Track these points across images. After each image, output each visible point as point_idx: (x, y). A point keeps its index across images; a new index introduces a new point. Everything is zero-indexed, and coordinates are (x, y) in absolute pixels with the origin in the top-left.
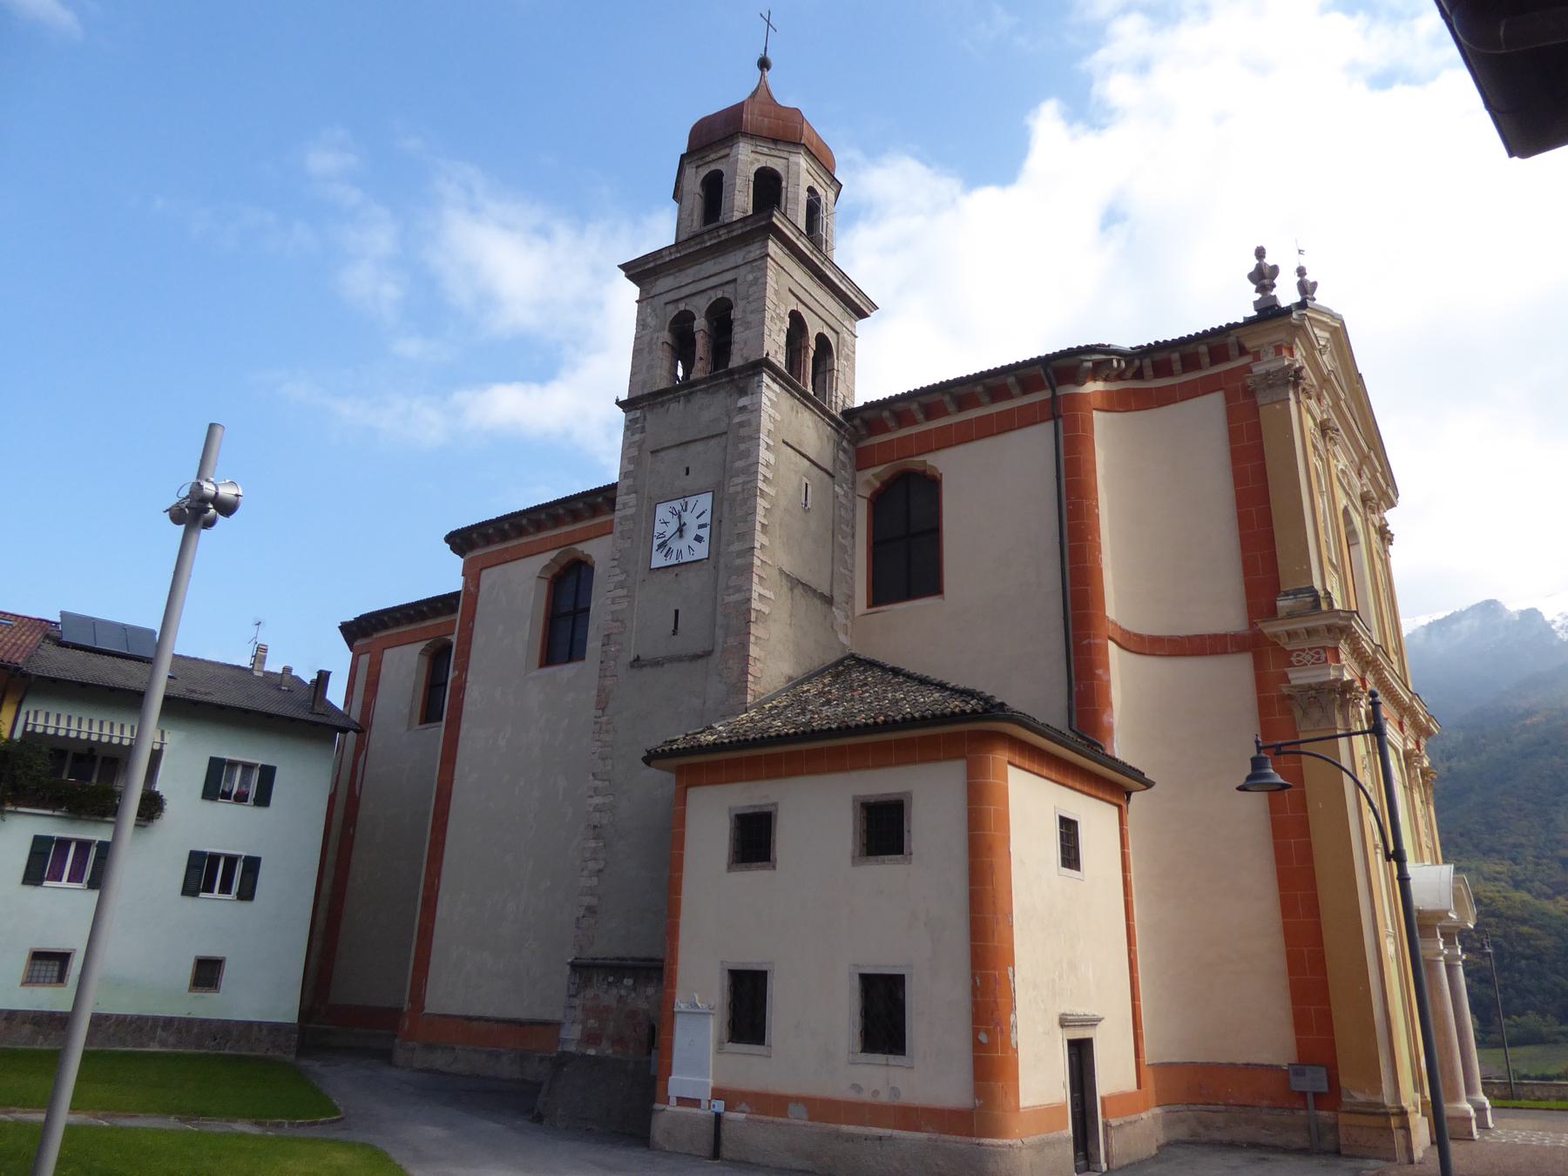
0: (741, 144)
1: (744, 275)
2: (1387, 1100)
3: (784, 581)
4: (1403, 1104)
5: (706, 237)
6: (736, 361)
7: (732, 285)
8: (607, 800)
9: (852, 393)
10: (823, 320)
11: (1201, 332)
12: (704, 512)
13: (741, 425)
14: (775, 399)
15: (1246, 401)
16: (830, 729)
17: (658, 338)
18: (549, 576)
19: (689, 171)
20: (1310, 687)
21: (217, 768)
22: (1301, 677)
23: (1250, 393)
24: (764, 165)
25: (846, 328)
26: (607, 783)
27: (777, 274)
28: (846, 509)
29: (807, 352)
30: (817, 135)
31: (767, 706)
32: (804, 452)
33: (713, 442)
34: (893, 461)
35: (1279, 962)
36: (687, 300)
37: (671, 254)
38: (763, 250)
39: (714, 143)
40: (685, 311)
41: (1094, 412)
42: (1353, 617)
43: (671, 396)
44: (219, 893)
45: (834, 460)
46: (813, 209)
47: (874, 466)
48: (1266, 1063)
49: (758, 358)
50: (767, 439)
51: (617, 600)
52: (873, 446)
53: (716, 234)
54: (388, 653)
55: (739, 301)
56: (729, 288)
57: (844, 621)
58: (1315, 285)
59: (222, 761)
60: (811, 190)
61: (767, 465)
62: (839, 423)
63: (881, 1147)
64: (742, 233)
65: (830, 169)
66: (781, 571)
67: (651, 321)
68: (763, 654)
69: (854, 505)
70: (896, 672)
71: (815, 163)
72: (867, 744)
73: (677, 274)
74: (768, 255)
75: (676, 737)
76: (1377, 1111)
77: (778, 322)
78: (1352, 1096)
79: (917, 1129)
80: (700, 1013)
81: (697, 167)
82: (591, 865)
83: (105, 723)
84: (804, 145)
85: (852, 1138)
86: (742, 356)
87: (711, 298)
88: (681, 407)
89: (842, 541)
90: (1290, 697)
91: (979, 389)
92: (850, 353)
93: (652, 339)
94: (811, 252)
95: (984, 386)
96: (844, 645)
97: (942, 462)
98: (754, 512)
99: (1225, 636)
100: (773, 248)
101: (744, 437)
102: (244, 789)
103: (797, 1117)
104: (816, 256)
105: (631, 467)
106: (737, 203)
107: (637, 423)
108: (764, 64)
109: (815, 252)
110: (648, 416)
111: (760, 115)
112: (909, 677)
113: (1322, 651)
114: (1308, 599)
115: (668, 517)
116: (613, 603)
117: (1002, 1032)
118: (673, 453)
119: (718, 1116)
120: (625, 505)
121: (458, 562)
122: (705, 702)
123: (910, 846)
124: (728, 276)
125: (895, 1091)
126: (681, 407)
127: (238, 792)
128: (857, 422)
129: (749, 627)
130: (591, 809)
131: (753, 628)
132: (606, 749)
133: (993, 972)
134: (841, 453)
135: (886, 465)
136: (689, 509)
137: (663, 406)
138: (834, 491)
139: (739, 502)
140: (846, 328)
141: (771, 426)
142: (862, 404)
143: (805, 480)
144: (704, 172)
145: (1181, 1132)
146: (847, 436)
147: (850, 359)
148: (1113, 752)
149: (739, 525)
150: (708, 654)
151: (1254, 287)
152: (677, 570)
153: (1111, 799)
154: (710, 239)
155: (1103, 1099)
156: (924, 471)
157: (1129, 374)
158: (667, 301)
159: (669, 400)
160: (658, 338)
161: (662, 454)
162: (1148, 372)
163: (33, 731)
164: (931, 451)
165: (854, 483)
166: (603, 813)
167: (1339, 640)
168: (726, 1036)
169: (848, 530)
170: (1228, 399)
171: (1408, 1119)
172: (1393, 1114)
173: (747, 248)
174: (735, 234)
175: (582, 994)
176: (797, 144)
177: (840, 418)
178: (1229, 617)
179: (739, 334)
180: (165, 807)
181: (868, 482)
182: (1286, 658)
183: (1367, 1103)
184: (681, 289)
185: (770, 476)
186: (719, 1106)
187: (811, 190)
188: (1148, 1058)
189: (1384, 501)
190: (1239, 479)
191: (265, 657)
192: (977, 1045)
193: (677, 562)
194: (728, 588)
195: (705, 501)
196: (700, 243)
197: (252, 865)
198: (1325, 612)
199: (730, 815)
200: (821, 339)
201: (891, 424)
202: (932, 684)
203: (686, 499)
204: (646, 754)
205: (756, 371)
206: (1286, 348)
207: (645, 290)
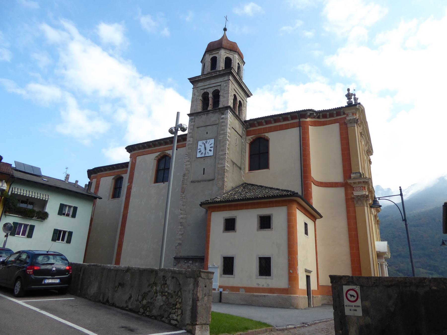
0: (222, 50)
1: (223, 84)
3: (232, 163)
5: (213, 73)
6: (221, 106)
7: (220, 86)
8: (184, 216)
10: (240, 97)
11: (327, 110)
13: (222, 122)
16: (253, 198)
17: (199, 98)
18: (157, 159)
19: (207, 56)
20: (359, 196)
21: (62, 207)
22: (356, 193)
23: (346, 124)
24: (228, 56)
26: (184, 212)
27: (232, 85)
28: (244, 146)
33: (214, 126)
34: (257, 134)
36: (207, 89)
37: (203, 77)
38: (228, 78)
43: (203, 113)
44: (61, 241)
46: (239, 68)
47: (251, 135)
50: (229, 126)
51: (187, 165)
54: (102, 179)
57: (243, 174)
58: (358, 98)
59: (63, 204)
60: (238, 63)
62: (244, 124)
63: (265, 298)
67: (197, 94)
68: (227, 180)
70: (262, 187)
71: (240, 57)
72: (255, 203)
73: (204, 82)
74: (230, 80)
75: (208, 200)
79: (274, 293)
80: (215, 268)
81: (210, 55)
82: (180, 233)
83: (33, 192)
85: (257, 296)
86: (222, 105)
88: (205, 116)
90: (354, 198)
91: (281, 118)
93: (197, 98)
94: (239, 80)
96: (243, 180)
97: (270, 135)
100: (231, 78)
101: (223, 125)
102: (68, 213)
103: (242, 292)
105: (191, 131)
107: (193, 120)
108: (225, 30)
112: (266, 187)
113: (361, 187)
114: (359, 175)
115: (202, 145)
116: (186, 166)
117: (295, 270)
118: (203, 128)
119: (221, 292)
120: (189, 141)
121: (129, 155)
122: (212, 192)
123: (272, 227)
125: (268, 285)
126: (205, 116)
127: (67, 213)
128: (248, 124)
129: (225, 174)
130: (180, 218)
131: (226, 174)
132: (184, 203)
133: (293, 256)
134: (243, 131)
137: (200, 116)
138: (242, 141)
139: (222, 142)
142: (249, 119)
144: (211, 56)
145: (325, 302)
146: (245, 127)
149: (222, 147)
150: (213, 180)
151: (347, 98)
152: (204, 158)
153: (313, 219)
154: (214, 74)
157: (316, 117)
158: (201, 89)
159: (202, 114)
160: (199, 98)
161: (200, 128)
162: (321, 117)
163: (14, 193)
164: (267, 132)
165: (246, 139)
166: (183, 220)
168: (222, 273)
169: (245, 151)
170: (340, 125)
174: (221, 73)
175: (177, 265)
176: (236, 52)
178: (339, 178)
179: (222, 99)
180: (49, 216)
181: (249, 139)
182: (353, 188)
185: (229, 135)
186: (221, 290)
187: (238, 63)
190: (342, 145)
191: (69, 178)
192: (289, 273)
193: (204, 156)
195: (212, 141)
197: (70, 234)
198: (363, 178)
199: (223, 219)
200: (240, 102)
201: (257, 125)
203: (207, 140)
204: (200, 203)
205: (226, 109)
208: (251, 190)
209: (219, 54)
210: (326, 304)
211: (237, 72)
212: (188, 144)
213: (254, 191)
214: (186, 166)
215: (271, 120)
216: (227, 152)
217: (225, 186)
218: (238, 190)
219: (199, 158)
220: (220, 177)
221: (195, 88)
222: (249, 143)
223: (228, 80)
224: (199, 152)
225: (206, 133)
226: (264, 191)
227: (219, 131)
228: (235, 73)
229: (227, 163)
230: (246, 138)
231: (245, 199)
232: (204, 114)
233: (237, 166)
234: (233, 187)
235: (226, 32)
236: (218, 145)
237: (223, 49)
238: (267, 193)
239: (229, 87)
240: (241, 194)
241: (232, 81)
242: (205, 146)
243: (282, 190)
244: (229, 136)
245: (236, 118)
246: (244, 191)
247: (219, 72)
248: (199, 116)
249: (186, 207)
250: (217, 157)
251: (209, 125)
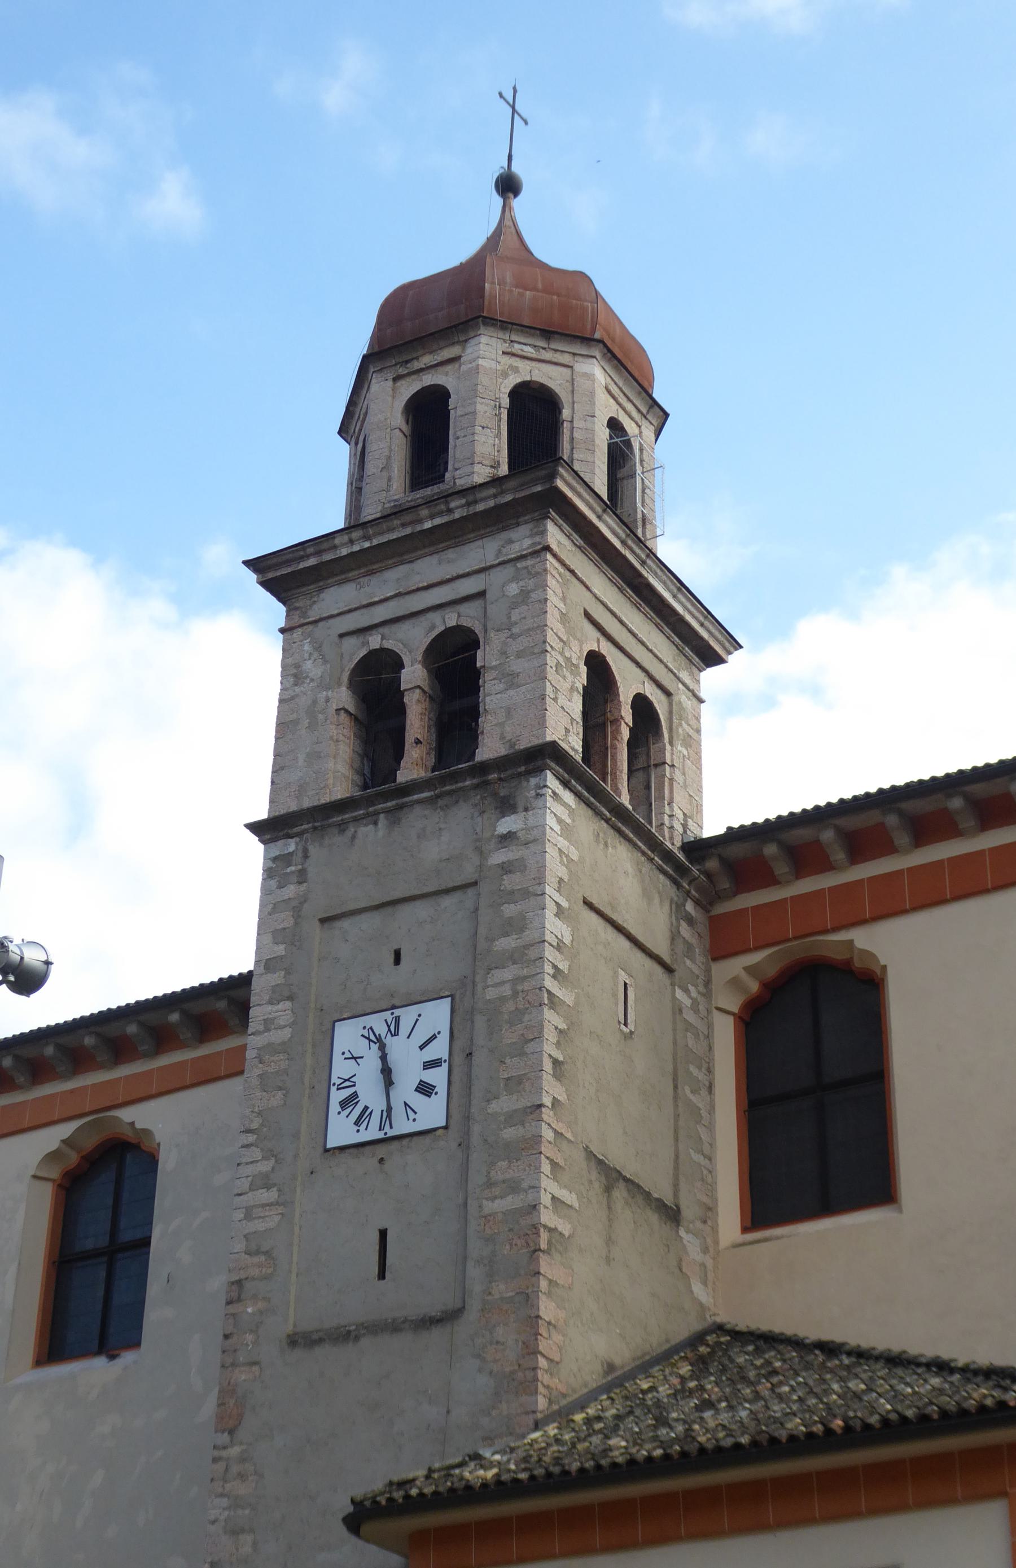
0: (484, 339)
3: (594, 1175)
5: (424, 512)
7: (478, 604)
9: (699, 809)
12: (434, 1037)
13: (507, 868)
14: (569, 821)
16: (738, 1446)
17: (327, 701)
18: (55, 1173)
19: (379, 386)
24: (528, 378)
25: (684, 685)
27: (565, 584)
28: (697, 1036)
29: (617, 731)
30: (621, 323)
31: (579, 1417)
34: (788, 940)
36: (385, 630)
37: (351, 542)
38: (537, 539)
39: (431, 334)
40: (382, 650)
45: (673, 939)
49: (536, 742)
50: (557, 897)
52: (743, 911)
53: (443, 507)
55: (492, 634)
56: (467, 609)
60: (614, 425)
61: (559, 947)
62: (680, 869)
64: (496, 507)
65: (646, 385)
67: (313, 668)
68: (562, 1315)
69: (710, 1026)
70: (829, 1349)
74: (547, 548)
75: (411, 1476)
77: (568, 674)
81: (395, 380)
84: (600, 341)
86: (502, 737)
87: (433, 627)
88: (381, 833)
89: (691, 1097)
92: (691, 732)
93: (315, 702)
94: (623, 543)
95: (968, 798)
96: (701, 1304)
98: (539, 1037)
100: (555, 535)
101: (512, 892)
104: (633, 552)
105: (280, 950)
106: (479, 449)
109: (630, 542)
110: (313, 850)
111: (517, 287)
112: (861, 1355)
115: (361, 1047)
116: (248, 1216)
118: (368, 923)
120: (268, 1024)
122: (448, 1412)
126: (381, 833)
131: (545, 1265)
132: (240, 1512)
134: (684, 925)
136: (404, 1030)
137: (342, 831)
138: (674, 998)
140: (684, 685)
141: (562, 872)
142: (721, 831)
143: (623, 977)
144: (410, 388)
146: (693, 892)
147: (693, 742)
149: (508, 1061)
150: (449, 1317)
152: (381, 1151)
154: (432, 517)
156: (849, 962)
159: (356, 820)
160: (327, 701)
161: (345, 924)
164: (863, 922)
165: (708, 983)
169: (701, 1076)
173: (505, 535)
174: (481, 507)
176: (587, 340)
181: (735, 983)
184: (373, 609)
185: (563, 966)
187: (614, 425)
193: (380, 1135)
194: (490, 1184)
196: (411, 523)
200: (642, 705)
201: (781, 868)
202: (919, 1365)
203: (397, 1012)
207: (296, 609)
208: (744, 1379)
209: (464, 368)
211: (605, 497)
212: (259, 1049)
213: (764, 1387)
214: (248, 1216)
215: (883, 824)
216: (551, 1089)
217: (542, 1362)
218: (653, 1389)
219: (345, 1156)
220: (501, 1289)
221: (300, 631)
222: (735, 1009)
223: (536, 553)
224: (344, 1104)
225: (392, 959)
226: (836, 1387)
227: (482, 931)
228: (580, 496)
229: (555, 1179)
230: (708, 971)
231: (684, 1454)
232: (372, 818)
233: (640, 1199)
234: (618, 1361)
235: (517, 204)
236: (480, 1040)
237: (491, 331)
238: (857, 1396)
239: (546, 600)
240: (662, 1421)
241: (563, 556)
242: (384, 1058)
243: (972, 1373)
244: (557, 973)
245: (611, 832)
246: (691, 1392)
247: (463, 501)
248: (335, 830)
249: (255, 1544)
250: (475, 1140)
251: (407, 894)
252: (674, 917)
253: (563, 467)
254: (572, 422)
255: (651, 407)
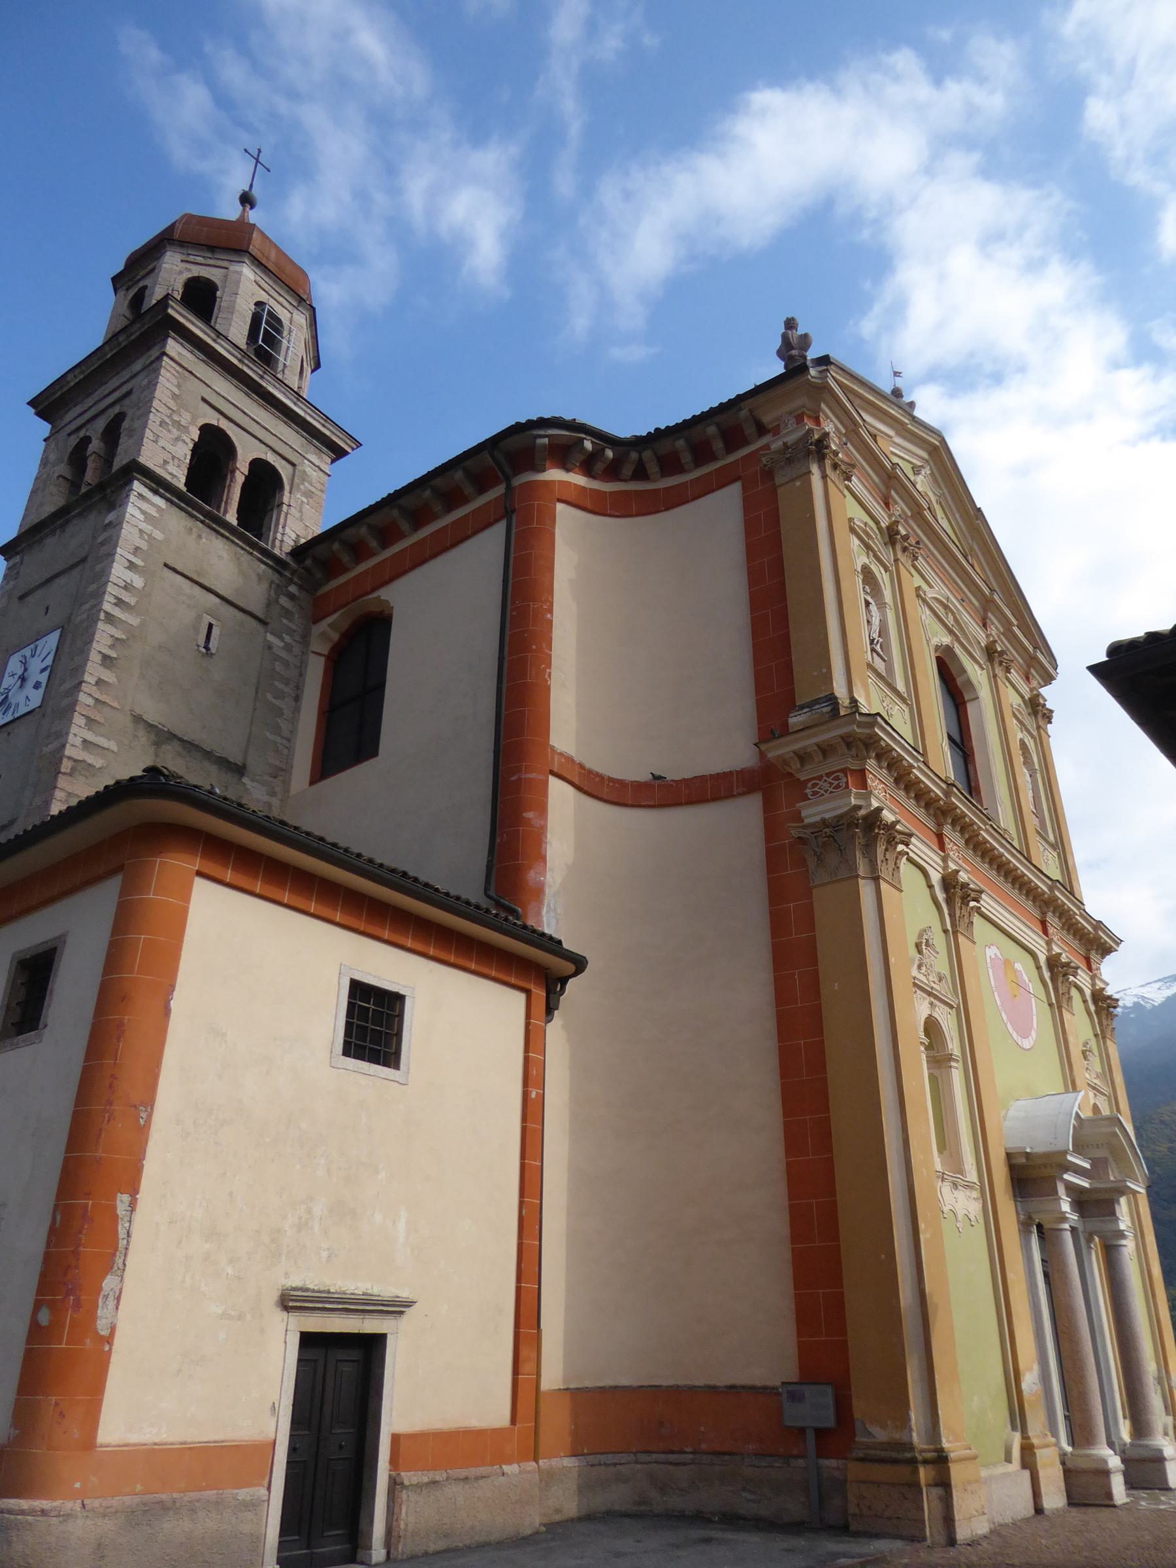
0: (168, 253)
2: (917, 1438)
4: (945, 1444)
12: (49, 653)
15: (765, 486)
22: (814, 812)
32: (207, 584)
35: (778, 1223)
41: (560, 507)
42: (875, 723)
48: (758, 1383)
66: (138, 719)
71: (270, 278)
76: (900, 1456)
78: (870, 1433)
94: (240, 361)
99: (731, 773)
109: (246, 362)
114: (824, 710)
117: (77, 1305)
124: (124, 390)
135: (342, 611)
145: (616, 1497)
146: (296, 580)
148: (540, 922)
154: (112, 350)
155: (396, 1439)
157: (627, 470)
161: (30, 598)
162: (653, 468)
167: (864, 759)
171: (948, 1468)
172: (926, 1462)
177: (289, 560)
179: (124, 443)
181: (323, 635)
182: (799, 790)
183: (889, 1443)
188: (553, 1375)
189: (1034, 668)
206: (809, 417)
210: (625, 1515)
222: (326, 652)
228: (193, 323)
252: (273, 592)
253: (172, 300)
254: (221, 298)
255: (300, 302)
